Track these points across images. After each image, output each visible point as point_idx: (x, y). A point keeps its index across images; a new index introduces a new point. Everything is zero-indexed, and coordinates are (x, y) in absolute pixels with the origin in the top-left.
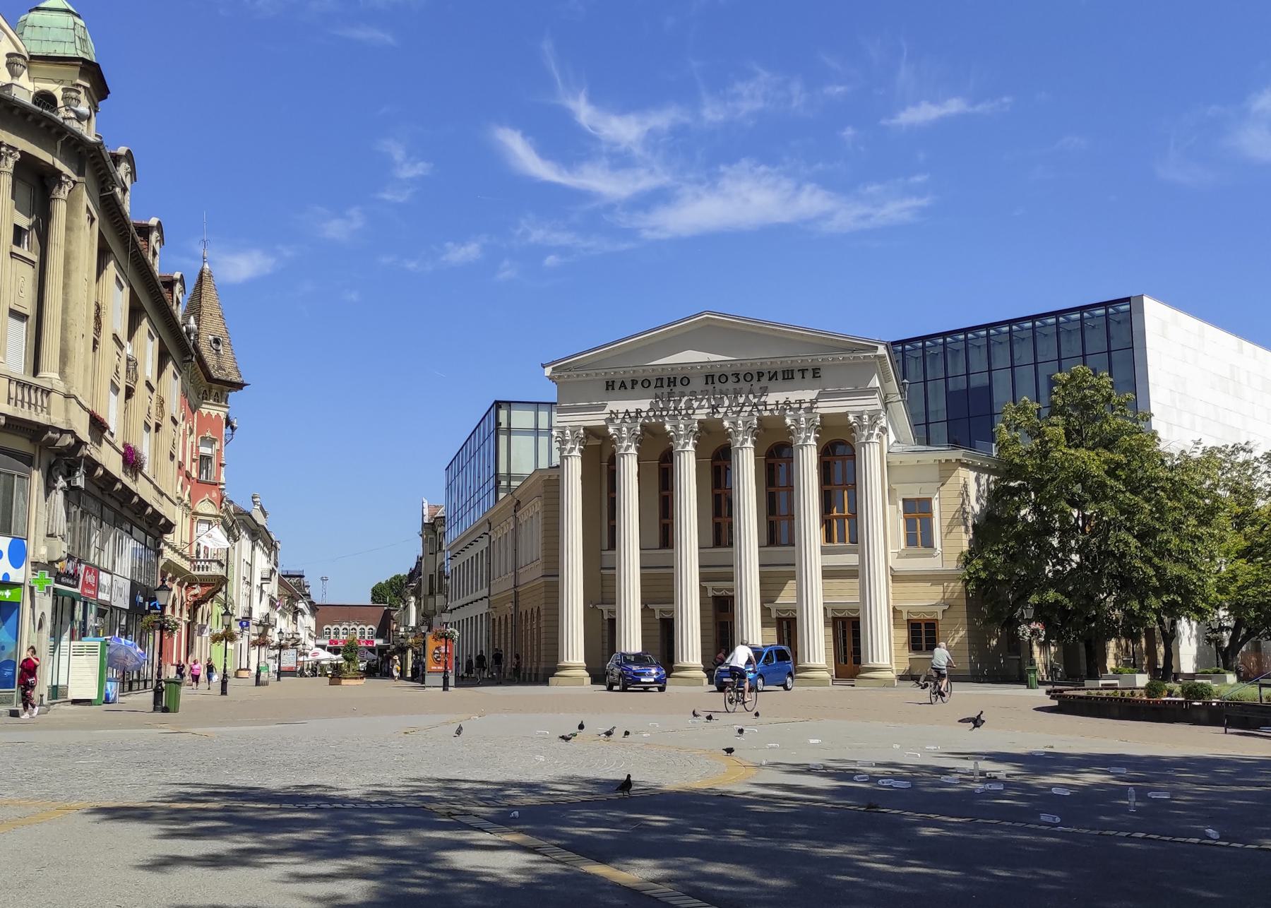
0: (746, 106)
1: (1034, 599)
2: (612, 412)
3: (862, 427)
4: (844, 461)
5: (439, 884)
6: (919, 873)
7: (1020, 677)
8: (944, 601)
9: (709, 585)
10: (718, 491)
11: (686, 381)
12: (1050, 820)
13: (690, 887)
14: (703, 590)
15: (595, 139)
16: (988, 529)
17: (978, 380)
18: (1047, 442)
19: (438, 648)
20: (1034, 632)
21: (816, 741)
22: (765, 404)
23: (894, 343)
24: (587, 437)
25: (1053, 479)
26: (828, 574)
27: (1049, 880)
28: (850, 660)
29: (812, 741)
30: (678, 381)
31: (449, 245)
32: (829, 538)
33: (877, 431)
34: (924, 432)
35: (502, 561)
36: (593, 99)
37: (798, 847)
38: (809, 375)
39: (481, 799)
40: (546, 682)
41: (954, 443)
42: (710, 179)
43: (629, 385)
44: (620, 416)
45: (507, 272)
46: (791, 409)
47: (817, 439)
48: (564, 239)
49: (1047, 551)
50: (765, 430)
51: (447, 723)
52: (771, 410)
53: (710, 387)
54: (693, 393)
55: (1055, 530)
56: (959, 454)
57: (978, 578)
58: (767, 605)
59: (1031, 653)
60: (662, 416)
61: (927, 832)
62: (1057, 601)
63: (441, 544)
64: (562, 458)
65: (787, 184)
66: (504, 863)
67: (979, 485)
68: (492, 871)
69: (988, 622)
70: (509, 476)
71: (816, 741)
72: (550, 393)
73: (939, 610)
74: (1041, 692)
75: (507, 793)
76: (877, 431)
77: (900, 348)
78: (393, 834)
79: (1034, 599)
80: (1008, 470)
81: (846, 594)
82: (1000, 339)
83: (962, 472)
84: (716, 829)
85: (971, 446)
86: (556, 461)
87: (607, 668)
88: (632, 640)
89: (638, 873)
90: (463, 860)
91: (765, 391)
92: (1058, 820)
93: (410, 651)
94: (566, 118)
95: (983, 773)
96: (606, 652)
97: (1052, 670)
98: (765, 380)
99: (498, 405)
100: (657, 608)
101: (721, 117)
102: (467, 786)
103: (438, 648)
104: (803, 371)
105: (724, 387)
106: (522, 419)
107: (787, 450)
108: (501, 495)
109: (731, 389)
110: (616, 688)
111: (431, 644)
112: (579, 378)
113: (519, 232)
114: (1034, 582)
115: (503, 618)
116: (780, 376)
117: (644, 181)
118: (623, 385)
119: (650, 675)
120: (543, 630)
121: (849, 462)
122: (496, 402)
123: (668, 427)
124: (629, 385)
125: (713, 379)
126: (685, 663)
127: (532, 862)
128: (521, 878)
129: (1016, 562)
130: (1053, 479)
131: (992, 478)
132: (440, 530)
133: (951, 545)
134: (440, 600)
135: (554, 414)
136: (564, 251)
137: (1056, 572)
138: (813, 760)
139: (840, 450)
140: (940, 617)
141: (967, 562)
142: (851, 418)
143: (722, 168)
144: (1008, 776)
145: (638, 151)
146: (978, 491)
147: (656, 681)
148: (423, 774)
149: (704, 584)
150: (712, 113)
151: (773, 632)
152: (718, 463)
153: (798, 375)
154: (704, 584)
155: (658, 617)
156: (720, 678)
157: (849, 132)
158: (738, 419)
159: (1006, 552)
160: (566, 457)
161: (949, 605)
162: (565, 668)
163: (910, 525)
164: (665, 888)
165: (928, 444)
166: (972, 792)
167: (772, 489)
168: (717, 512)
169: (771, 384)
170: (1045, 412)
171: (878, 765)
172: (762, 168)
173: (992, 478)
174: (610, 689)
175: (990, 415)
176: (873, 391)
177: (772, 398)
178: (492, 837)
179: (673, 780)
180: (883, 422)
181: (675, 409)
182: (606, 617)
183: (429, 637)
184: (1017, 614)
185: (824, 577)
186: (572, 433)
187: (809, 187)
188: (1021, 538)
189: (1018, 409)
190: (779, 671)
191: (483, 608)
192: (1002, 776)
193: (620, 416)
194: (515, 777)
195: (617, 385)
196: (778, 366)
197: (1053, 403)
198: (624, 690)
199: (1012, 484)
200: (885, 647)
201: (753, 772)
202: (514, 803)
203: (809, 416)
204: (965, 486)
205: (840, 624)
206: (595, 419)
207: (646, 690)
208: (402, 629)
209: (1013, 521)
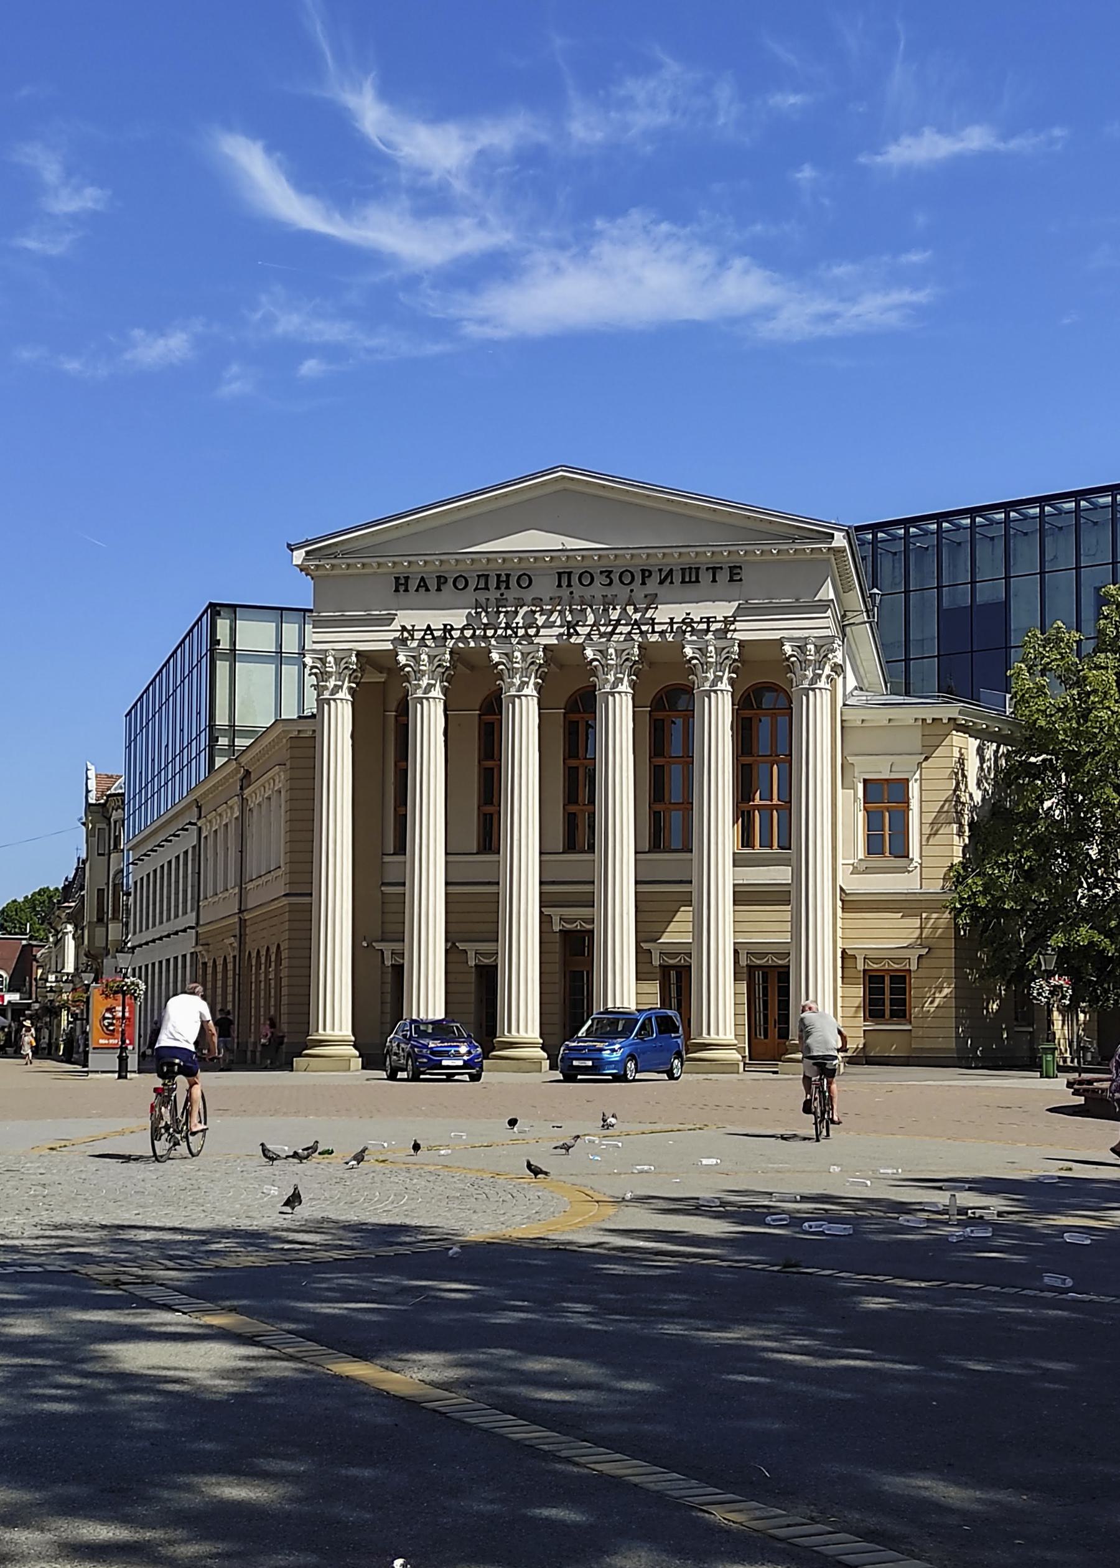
0: (642, 120)
1: (1057, 940)
2: (404, 629)
3: (804, 663)
4: (774, 717)
5: (96, 1396)
6: (854, 1369)
7: (1029, 1060)
8: (921, 941)
9: (555, 912)
10: (573, 763)
11: (526, 580)
12: (1058, 1284)
13: (499, 1395)
14: (545, 920)
15: (387, 162)
16: (993, 829)
17: (989, 592)
18: (1088, 694)
19: (110, 1010)
20: (1055, 990)
21: (713, 1161)
22: (652, 622)
23: (858, 529)
24: (362, 669)
25: (1096, 752)
26: (743, 897)
27: (1046, 1374)
28: (774, 1032)
29: (705, 1162)
30: (513, 582)
31: (138, 333)
32: (746, 840)
33: (827, 670)
34: (902, 678)
35: (219, 871)
36: (387, 93)
37: (673, 1329)
38: (723, 576)
39: (171, 1258)
40: (290, 1067)
41: (948, 690)
42: (579, 243)
43: (432, 584)
44: (418, 635)
45: (236, 383)
46: (693, 631)
47: (732, 682)
48: (334, 331)
49: (1079, 865)
50: (651, 664)
51: (122, 1133)
52: (662, 633)
53: (565, 593)
54: (537, 601)
55: (1093, 831)
56: (952, 711)
57: (974, 907)
58: (645, 946)
59: (1050, 1022)
60: (485, 637)
61: (875, 1303)
62: (1091, 943)
63: (117, 839)
64: (321, 702)
65: (703, 257)
66: (205, 1362)
67: (982, 760)
68: (182, 1374)
69: (987, 975)
70: (233, 730)
71: (713, 1161)
72: (303, 594)
73: (914, 955)
74: (1060, 1082)
75: (214, 1247)
76: (827, 670)
77: (872, 540)
78: (22, 1315)
79: (1057, 940)
80: (1031, 738)
81: (770, 928)
82: (1025, 527)
83: (958, 739)
84: (545, 1302)
85: (973, 696)
86: (311, 706)
87: (389, 1043)
88: (429, 999)
89: (416, 1374)
90: (137, 1357)
91: (652, 601)
92: (1069, 1283)
93: (64, 1013)
94: (340, 124)
95: (962, 1211)
96: (388, 1018)
97: (1079, 1050)
98: (652, 586)
99: (215, 610)
100: (470, 947)
101: (599, 136)
102: (149, 1236)
103: (110, 1010)
104: (714, 570)
105: (588, 592)
106: (255, 635)
107: (685, 697)
108: (219, 761)
109: (598, 596)
110: (400, 1075)
111: (99, 1004)
112: (347, 573)
113: (258, 316)
114: (1044, 924)
115: (220, 961)
116: (677, 577)
117: (470, 239)
118: (423, 584)
119: (457, 1055)
120: (284, 982)
121: (782, 720)
122: (211, 605)
123: (495, 657)
124: (432, 584)
125: (570, 578)
126: (514, 1036)
127: (248, 1358)
128: (230, 1386)
129: (1032, 881)
130: (1096, 752)
131: (1003, 749)
132: (115, 815)
133: (935, 854)
134: (114, 930)
135: (309, 628)
136: (332, 352)
137: (1093, 898)
138: (705, 1192)
139: (768, 699)
140: (914, 967)
141: (960, 880)
142: (788, 649)
143: (599, 224)
144: (1000, 1214)
145: (459, 186)
146: (981, 769)
147: (466, 1065)
148: (77, 1217)
149: (547, 911)
150: (585, 129)
151: (654, 987)
152: (574, 717)
153: (706, 577)
154: (547, 911)
155: (472, 963)
156: (568, 1060)
157: (806, 173)
158: (608, 645)
159: (1019, 866)
160: (328, 701)
161: (928, 947)
162: (320, 1043)
163: (873, 821)
164: (458, 1398)
165: (907, 693)
166: (944, 1239)
167: (659, 761)
168: (571, 796)
169: (663, 591)
170: (1088, 647)
171: (804, 1199)
172: (665, 227)
173: (1003, 749)
174: (392, 1077)
175: (1004, 650)
176: (825, 605)
177: (663, 614)
178: (185, 1318)
179: (480, 1225)
180: (838, 657)
181: (508, 626)
182: (388, 963)
183: (96, 990)
184: (1030, 964)
185: (736, 903)
186: (338, 661)
187: (739, 263)
188: (1042, 845)
189: (1047, 641)
190: (661, 1049)
191: (186, 945)
192: (991, 1215)
193: (418, 635)
194: (229, 1222)
195: (413, 584)
196: (675, 560)
197: (1101, 632)
198: (415, 1078)
199: (1033, 760)
200: (828, 1009)
201: (611, 1210)
202: (225, 1263)
203: (721, 644)
204: (961, 761)
205: (758, 975)
206: (377, 640)
207: (449, 1078)
208: (52, 978)
209: (1032, 816)
